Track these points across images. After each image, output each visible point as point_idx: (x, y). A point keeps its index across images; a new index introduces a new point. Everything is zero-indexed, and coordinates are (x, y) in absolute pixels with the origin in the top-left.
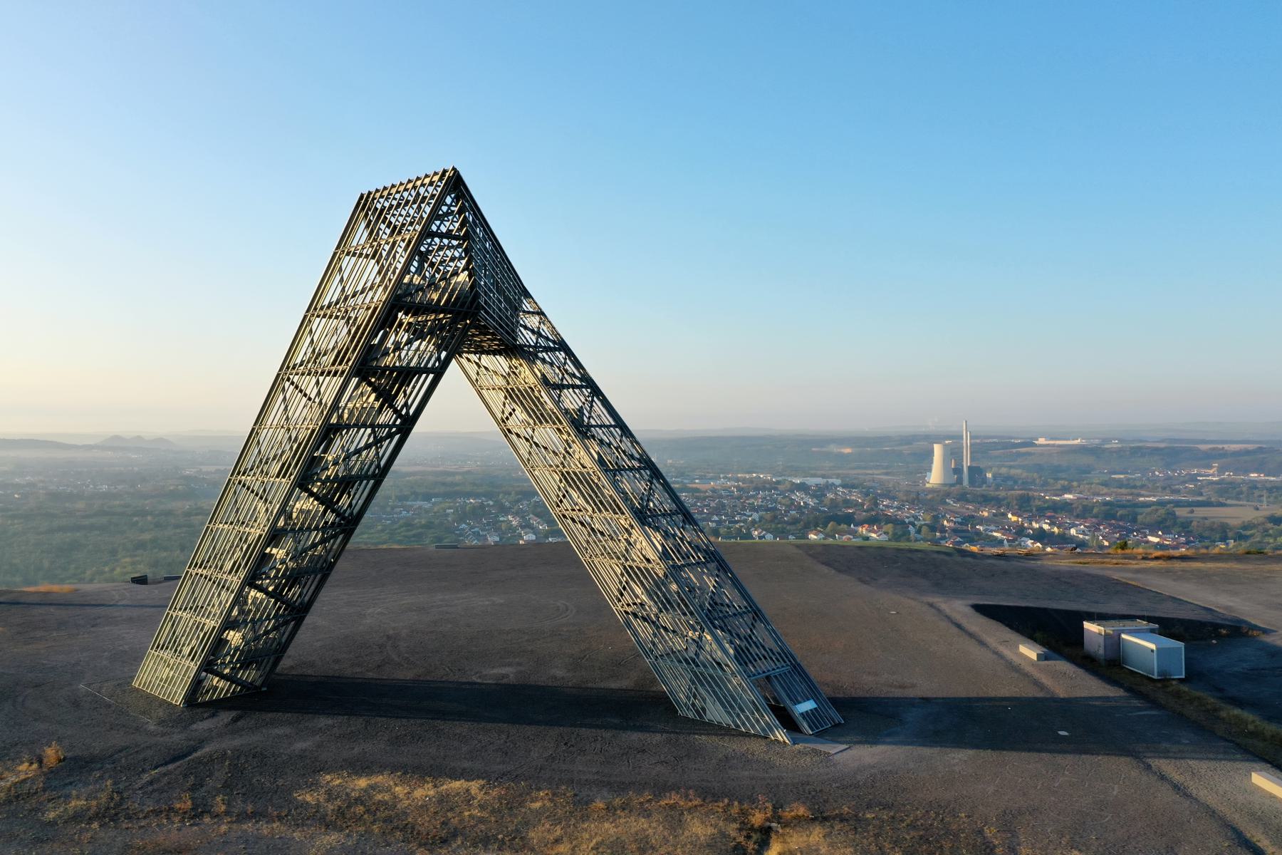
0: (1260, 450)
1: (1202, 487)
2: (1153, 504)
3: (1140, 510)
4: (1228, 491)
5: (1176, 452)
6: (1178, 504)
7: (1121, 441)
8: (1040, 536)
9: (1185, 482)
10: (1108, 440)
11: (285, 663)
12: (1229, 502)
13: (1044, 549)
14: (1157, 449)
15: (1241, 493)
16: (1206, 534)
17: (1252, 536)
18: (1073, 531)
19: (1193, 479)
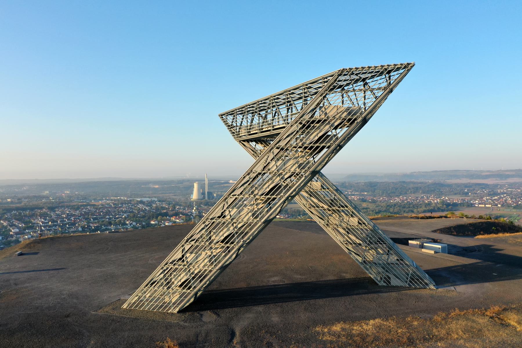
16: (294, 214)
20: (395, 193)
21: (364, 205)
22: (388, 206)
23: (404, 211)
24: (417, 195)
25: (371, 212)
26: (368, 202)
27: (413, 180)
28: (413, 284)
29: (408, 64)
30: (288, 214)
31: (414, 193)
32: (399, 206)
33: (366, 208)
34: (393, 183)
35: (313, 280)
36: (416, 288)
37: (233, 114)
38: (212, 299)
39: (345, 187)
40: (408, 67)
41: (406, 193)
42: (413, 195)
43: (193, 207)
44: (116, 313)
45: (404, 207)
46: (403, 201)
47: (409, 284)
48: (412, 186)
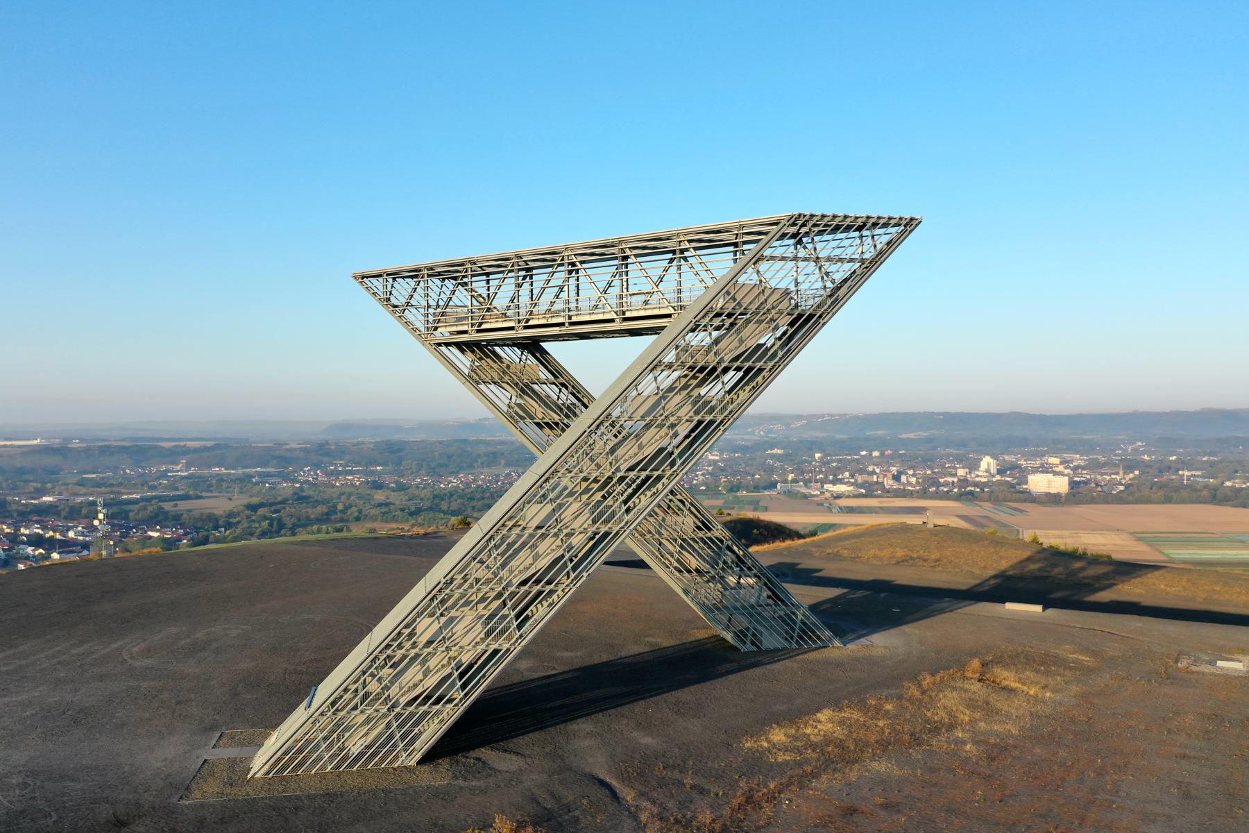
0: (217, 446)
1: (175, 481)
2: (136, 502)
3: (127, 507)
4: (200, 486)
5: (141, 450)
6: (162, 499)
7: (82, 440)
8: (37, 541)
9: (159, 478)
10: (70, 440)
11: (818, 380)
12: (204, 494)
13: (48, 557)
14: (124, 448)
15: (211, 486)
16: (199, 524)
17: (239, 522)
18: (71, 534)
19: (164, 475)
20: (447, 466)
21: (380, 496)
22: (436, 496)
23: (473, 508)
24: (495, 470)
25: (398, 513)
26: (388, 488)
27: (483, 437)
28: (806, 642)
29: (912, 219)
30: (182, 526)
31: (489, 466)
32: (460, 497)
33: (387, 504)
34: (441, 442)
35: (605, 658)
36: (811, 650)
37: (416, 276)
38: (499, 716)
39: (328, 454)
40: (910, 224)
41: (471, 466)
42: (486, 470)
43: (97, 512)
44: (239, 793)
45: (472, 499)
46: (468, 484)
47: (797, 642)
48: (482, 449)
